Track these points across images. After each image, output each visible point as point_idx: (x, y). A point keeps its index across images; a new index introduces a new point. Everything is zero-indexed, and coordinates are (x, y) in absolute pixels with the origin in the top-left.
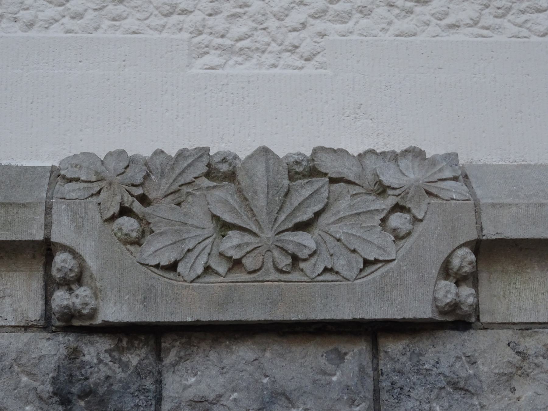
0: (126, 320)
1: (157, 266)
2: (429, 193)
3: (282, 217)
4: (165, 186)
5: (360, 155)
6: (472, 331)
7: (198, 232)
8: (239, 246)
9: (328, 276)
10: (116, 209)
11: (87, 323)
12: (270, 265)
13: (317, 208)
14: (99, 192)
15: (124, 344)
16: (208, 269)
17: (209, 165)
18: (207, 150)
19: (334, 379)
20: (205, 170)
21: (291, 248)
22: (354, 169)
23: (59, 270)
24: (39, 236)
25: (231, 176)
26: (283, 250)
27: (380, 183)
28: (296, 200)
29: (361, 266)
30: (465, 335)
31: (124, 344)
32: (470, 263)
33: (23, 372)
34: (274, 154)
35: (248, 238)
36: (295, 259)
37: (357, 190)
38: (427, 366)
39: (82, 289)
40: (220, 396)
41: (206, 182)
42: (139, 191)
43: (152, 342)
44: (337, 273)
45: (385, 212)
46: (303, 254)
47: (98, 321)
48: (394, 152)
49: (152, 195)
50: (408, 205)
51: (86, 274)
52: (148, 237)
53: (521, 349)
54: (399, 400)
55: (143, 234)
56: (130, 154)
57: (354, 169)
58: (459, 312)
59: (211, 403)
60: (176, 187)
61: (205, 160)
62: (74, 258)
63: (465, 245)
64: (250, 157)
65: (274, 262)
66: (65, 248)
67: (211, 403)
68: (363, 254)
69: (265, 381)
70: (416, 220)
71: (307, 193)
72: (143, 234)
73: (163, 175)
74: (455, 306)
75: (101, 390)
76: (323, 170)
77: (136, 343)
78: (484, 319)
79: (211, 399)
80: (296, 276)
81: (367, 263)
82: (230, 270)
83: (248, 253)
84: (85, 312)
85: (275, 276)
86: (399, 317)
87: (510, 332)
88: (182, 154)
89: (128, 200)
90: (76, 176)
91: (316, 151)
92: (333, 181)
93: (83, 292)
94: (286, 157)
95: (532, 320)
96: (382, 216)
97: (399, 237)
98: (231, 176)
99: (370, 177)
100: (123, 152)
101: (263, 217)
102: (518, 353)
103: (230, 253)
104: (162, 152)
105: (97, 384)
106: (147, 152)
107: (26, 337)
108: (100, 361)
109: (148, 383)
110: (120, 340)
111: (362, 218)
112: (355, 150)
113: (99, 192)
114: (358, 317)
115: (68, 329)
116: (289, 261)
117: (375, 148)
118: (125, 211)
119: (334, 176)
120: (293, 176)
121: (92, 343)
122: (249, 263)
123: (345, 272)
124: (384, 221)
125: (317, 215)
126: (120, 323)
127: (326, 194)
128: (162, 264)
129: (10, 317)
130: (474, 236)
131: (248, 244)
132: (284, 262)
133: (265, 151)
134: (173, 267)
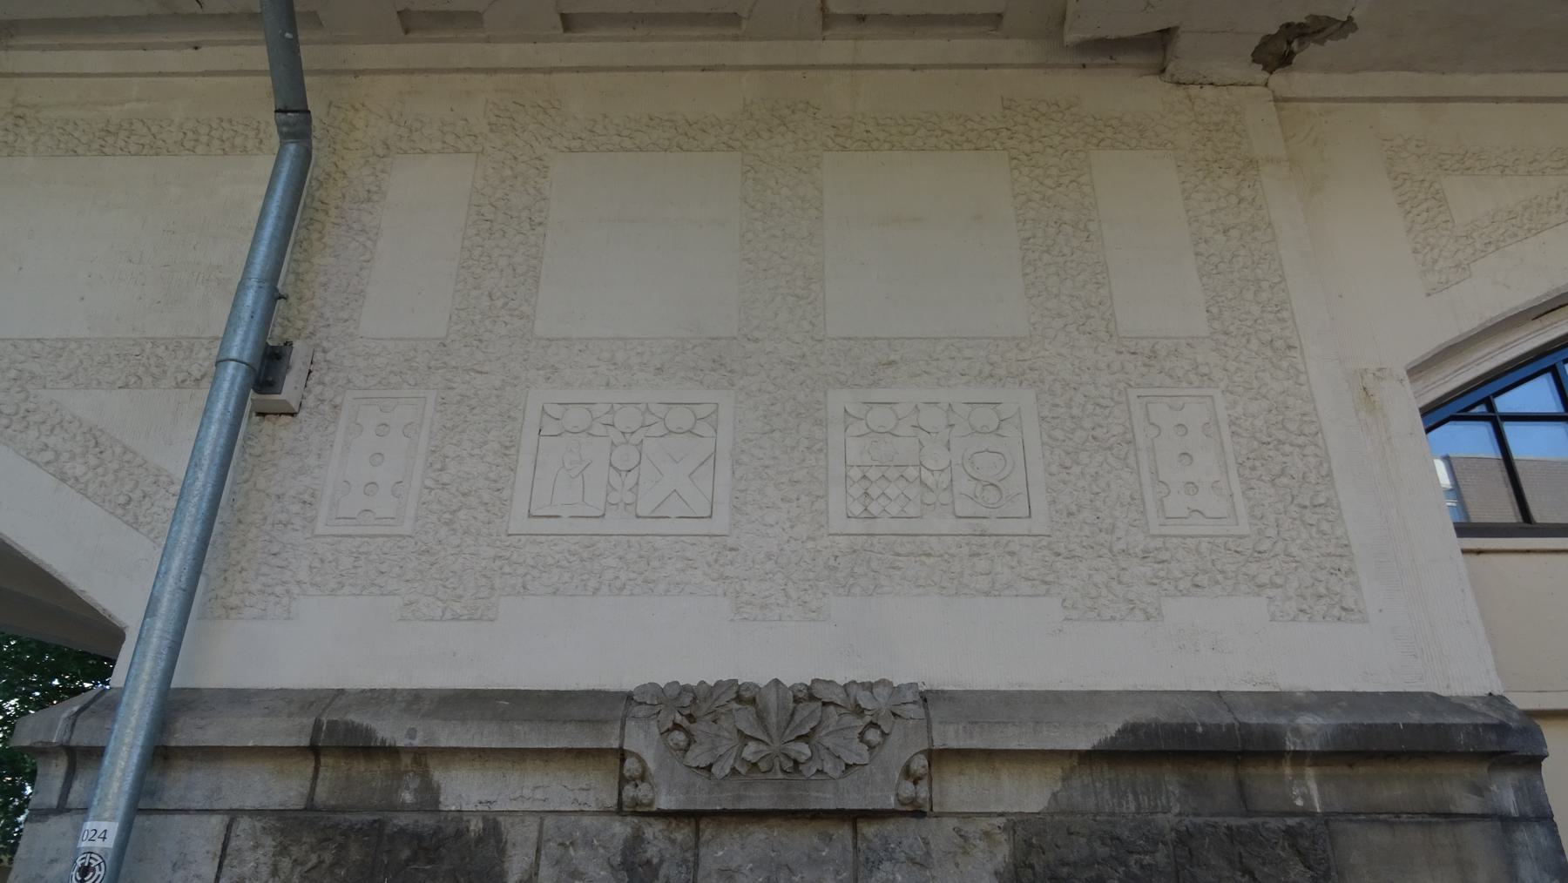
0: (673, 808)
1: (698, 768)
2: (894, 714)
3: (788, 731)
4: (705, 707)
5: (845, 685)
6: (927, 818)
7: (422, 733)
8: (755, 753)
9: (820, 777)
10: (670, 725)
11: (647, 809)
12: (778, 767)
13: (812, 725)
14: (659, 713)
15: (674, 825)
16: (734, 771)
17: (737, 692)
18: (736, 681)
19: (824, 854)
20: (734, 696)
21: (793, 755)
22: (841, 696)
23: (629, 770)
24: (616, 745)
25: (753, 701)
26: (787, 756)
27: (858, 705)
28: (798, 718)
29: (844, 768)
30: (922, 822)
31: (674, 825)
32: (924, 767)
33: (600, 845)
34: (782, 684)
35: (763, 747)
36: (796, 763)
37: (843, 711)
38: (892, 846)
39: (644, 784)
40: (740, 866)
41: (735, 706)
42: (687, 712)
43: (693, 824)
44: (826, 773)
45: (862, 728)
46: (802, 759)
47: (654, 809)
48: (870, 683)
49: (697, 714)
50: (879, 723)
51: (647, 774)
52: (693, 746)
53: (963, 833)
54: (871, 871)
55: (689, 745)
56: (681, 684)
57: (841, 696)
58: (916, 804)
59: (733, 872)
60: (713, 708)
61: (735, 689)
62: (639, 762)
63: (921, 752)
64: (766, 686)
65: (781, 766)
66: (633, 754)
67: (733, 872)
68: (845, 759)
69: (773, 855)
70: (884, 735)
71: (806, 713)
72: (689, 745)
73: (705, 700)
74: (913, 800)
75: (655, 861)
76: (818, 696)
77: (682, 825)
78: (935, 809)
79: (732, 868)
80: (796, 776)
81: (847, 766)
82: (749, 771)
83: (762, 758)
84: (644, 801)
85: (780, 775)
86: (871, 808)
87: (956, 820)
88: (718, 684)
89: (679, 718)
90: (644, 700)
91: (813, 681)
92: (825, 704)
93: (644, 787)
94: (792, 688)
95: (972, 810)
96: (860, 730)
97: (871, 747)
98: (812, 698)
99: (852, 701)
100: (677, 682)
101: (773, 731)
102: (961, 836)
103: (750, 758)
104: (704, 682)
105: (652, 857)
106: (694, 683)
107: (604, 819)
108: (655, 838)
109: (689, 855)
110: (670, 823)
111: (845, 732)
112: (841, 681)
113: (659, 713)
114: (840, 807)
115: (635, 813)
116: (791, 764)
117: (856, 679)
118: (677, 726)
119: (826, 700)
120: (797, 700)
121: (650, 825)
122: (763, 766)
123: (831, 773)
124: (862, 734)
125: (813, 729)
126: (669, 810)
127: (820, 714)
128: (701, 766)
129: (593, 805)
130: (926, 746)
131: (761, 751)
132: (788, 765)
133: (777, 682)
134: (709, 768)
